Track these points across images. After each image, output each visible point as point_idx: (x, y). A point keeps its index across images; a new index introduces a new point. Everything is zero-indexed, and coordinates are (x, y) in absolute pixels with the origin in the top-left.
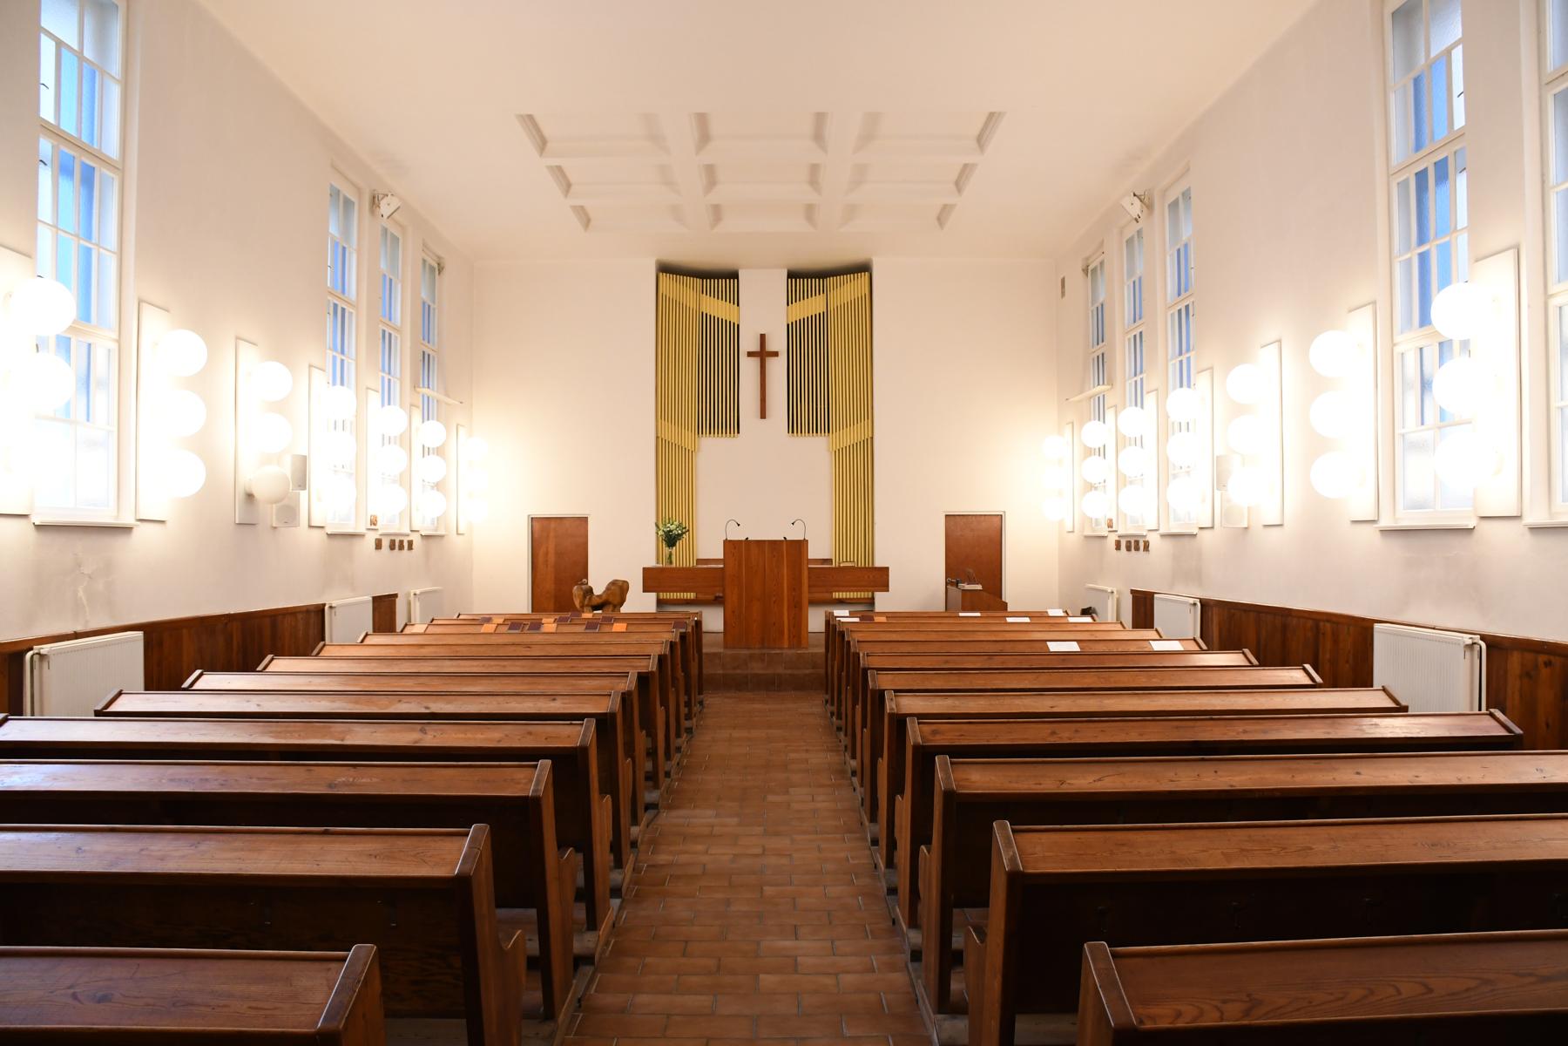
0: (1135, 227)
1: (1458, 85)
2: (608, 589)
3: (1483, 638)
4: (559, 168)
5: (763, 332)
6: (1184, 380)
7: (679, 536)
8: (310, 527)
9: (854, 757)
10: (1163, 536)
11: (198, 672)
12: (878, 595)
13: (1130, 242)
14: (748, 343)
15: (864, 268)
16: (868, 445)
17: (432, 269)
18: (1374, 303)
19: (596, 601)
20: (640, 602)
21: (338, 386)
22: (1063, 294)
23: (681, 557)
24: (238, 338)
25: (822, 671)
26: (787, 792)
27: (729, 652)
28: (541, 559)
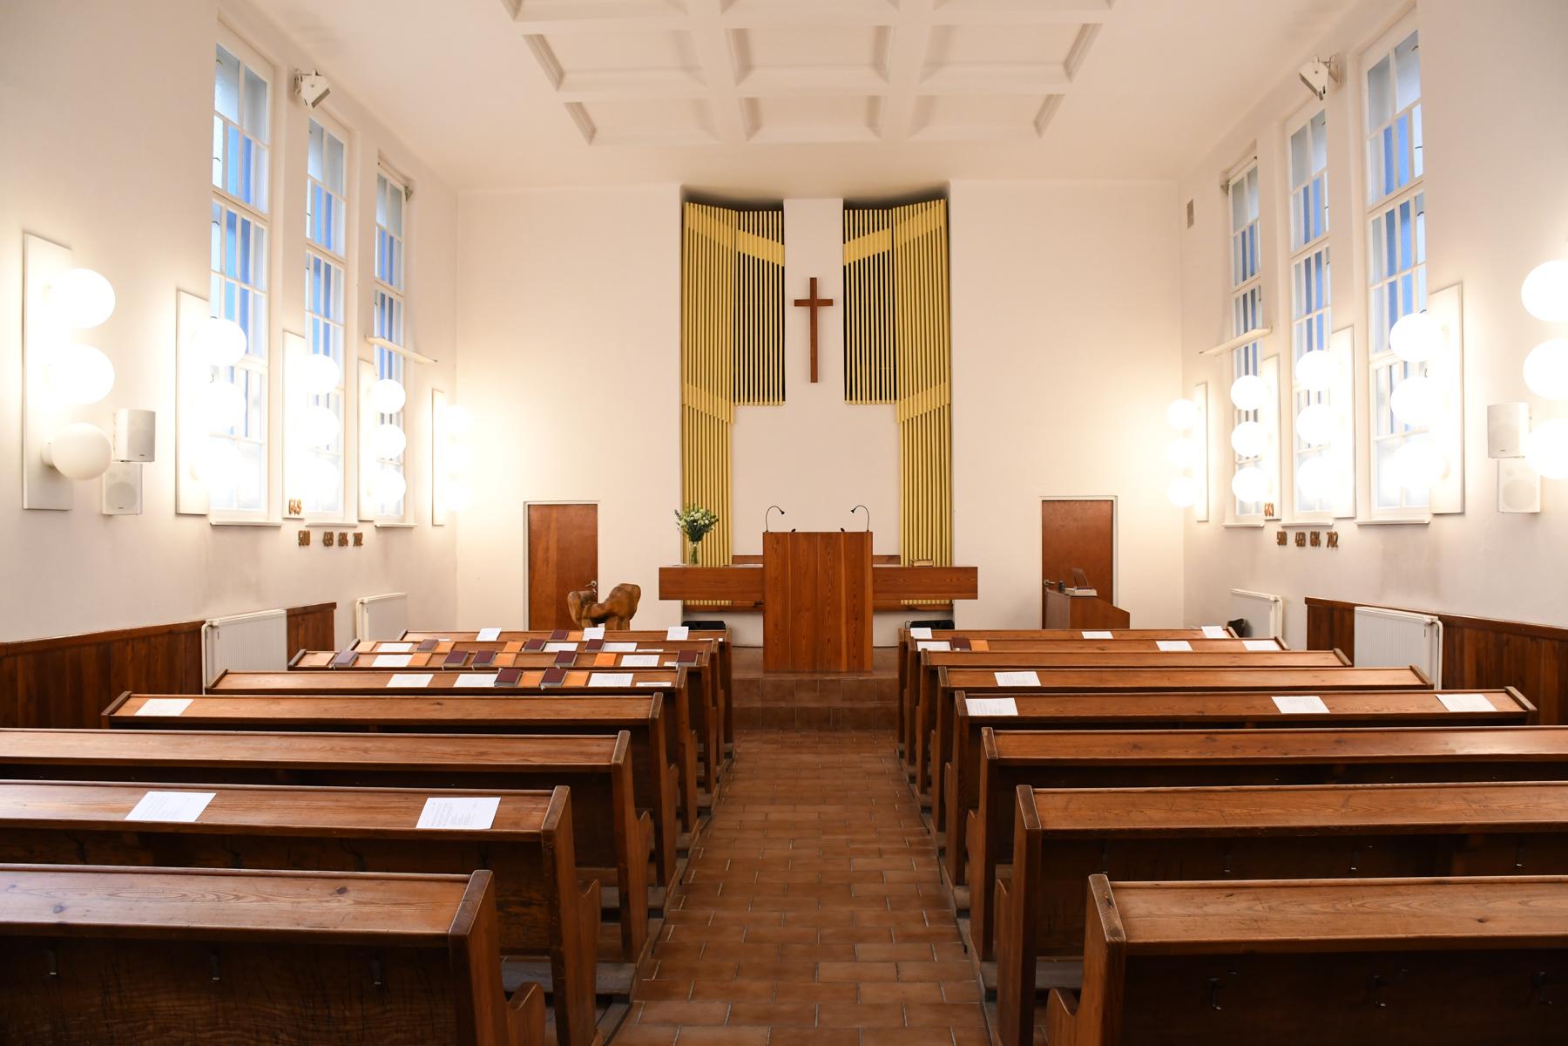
0: (1316, 107)
1: (1418, 139)
2: (612, 596)
3: (1441, 618)
4: (541, 38)
5: (817, 278)
6: (1313, 339)
7: (706, 528)
8: (178, 514)
9: (959, 880)
10: (1360, 526)
11: (126, 694)
12: (959, 604)
13: (1299, 138)
14: (796, 289)
15: (937, 195)
16: (944, 414)
17: (396, 192)
18: (1460, 283)
19: (596, 611)
20: (661, 616)
21: (321, 355)
22: (1190, 222)
23: (710, 554)
24: (25, 232)
25: (896, 705)
26: (852, 956)
27: (771, 678)
28: (540, 554)
